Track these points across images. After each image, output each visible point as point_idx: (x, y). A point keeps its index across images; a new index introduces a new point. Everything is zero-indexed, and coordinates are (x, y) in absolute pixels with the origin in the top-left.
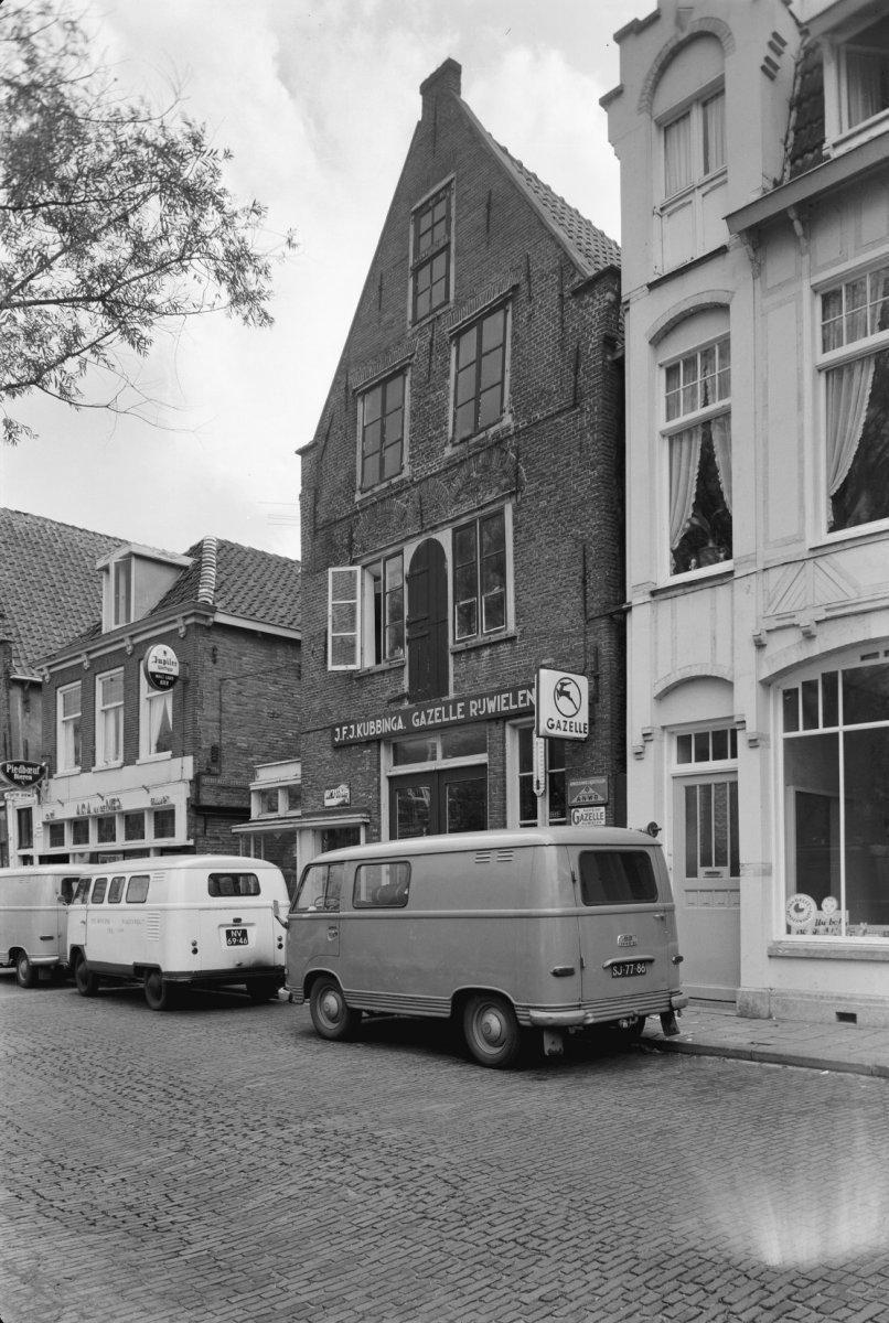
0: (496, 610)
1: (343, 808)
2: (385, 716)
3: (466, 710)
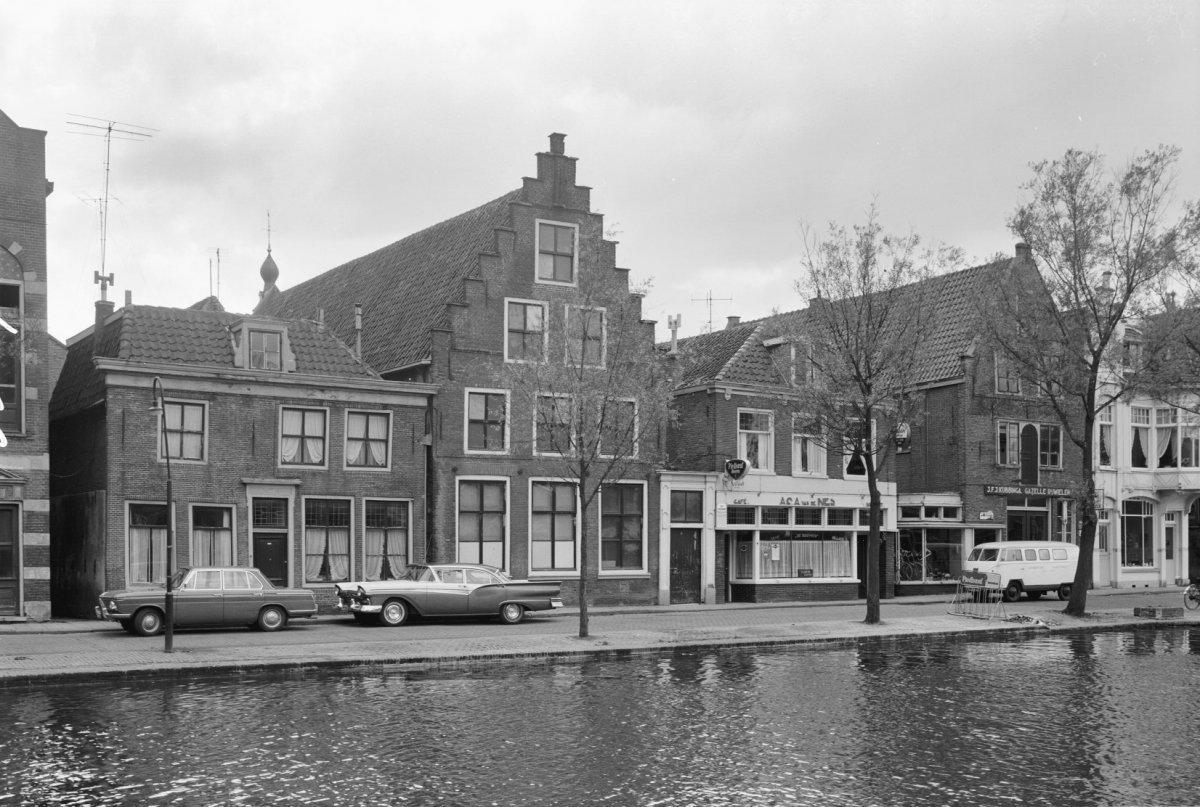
0: (1054, 460)
1: (990, 521)
2: (1014, 486)
3: (1046, 492)
